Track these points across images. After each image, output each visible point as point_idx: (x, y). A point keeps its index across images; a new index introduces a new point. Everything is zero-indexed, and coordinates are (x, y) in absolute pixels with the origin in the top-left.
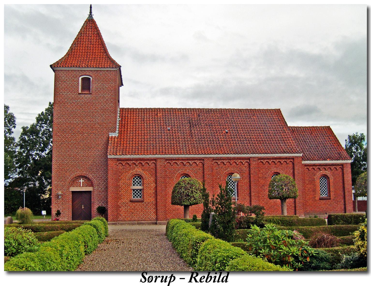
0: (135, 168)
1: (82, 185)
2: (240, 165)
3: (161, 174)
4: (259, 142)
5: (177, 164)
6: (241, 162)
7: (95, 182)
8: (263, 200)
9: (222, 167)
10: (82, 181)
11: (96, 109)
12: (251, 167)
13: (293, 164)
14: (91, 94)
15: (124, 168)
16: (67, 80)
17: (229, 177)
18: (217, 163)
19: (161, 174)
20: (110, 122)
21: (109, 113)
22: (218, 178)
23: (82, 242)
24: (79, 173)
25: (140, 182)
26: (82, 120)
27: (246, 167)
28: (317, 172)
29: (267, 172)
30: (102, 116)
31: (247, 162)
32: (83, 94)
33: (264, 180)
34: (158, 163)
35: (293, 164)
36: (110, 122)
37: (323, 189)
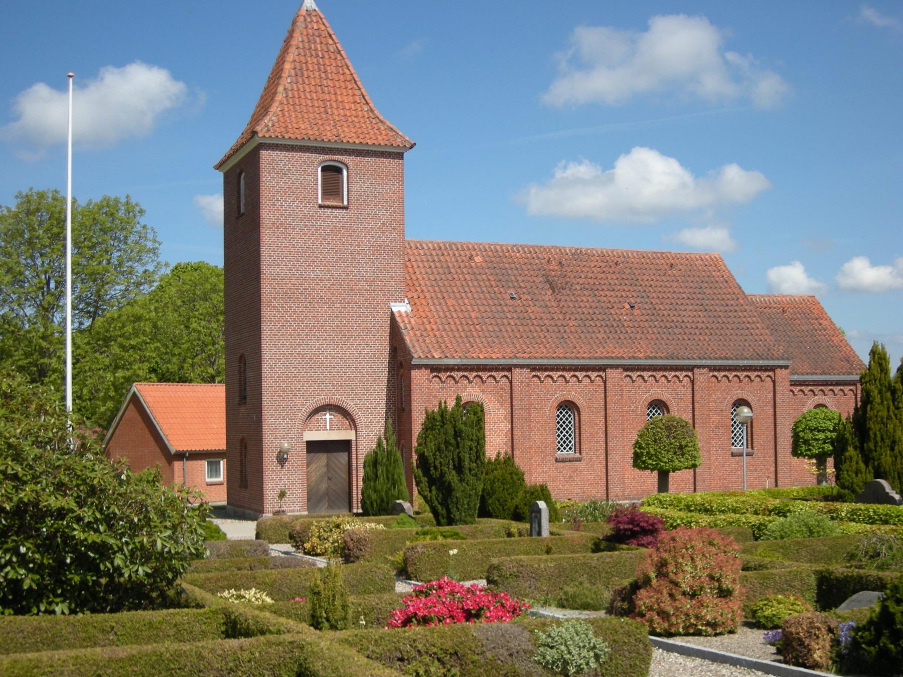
0: (466, 387)
1: (328, 427)
2: (675, 383)
3: (521, 400)
4: (425, 320)
5: (552, 378)
6: (675, 376)
7: (361, 418)
8: (717, 459)
9: (639, 387)
10: (328, 416)
11: (359, 246)
12: (696, 388)
13: (774, 382)
14: (346, 208)
15: (443, 388)
16: (289, 170)
17: (564, 413)
18: (630, 377)
19: (521, 400)
20: (392, 278)
21: (388, 255)
22: (633, 411)
23: (857, 476)
24: (322, 399)
25: (570, 416)
26: (329, 271)
27: (684, 386)
28: (808, 399)
29: (725, 399)
30: (373, 262)
31: (600, 376)
32: (328, 207)
33: (719, 415)
34: (515, 376)
35: (774, 382)
36: (392, 278)
37: (564, 436)
